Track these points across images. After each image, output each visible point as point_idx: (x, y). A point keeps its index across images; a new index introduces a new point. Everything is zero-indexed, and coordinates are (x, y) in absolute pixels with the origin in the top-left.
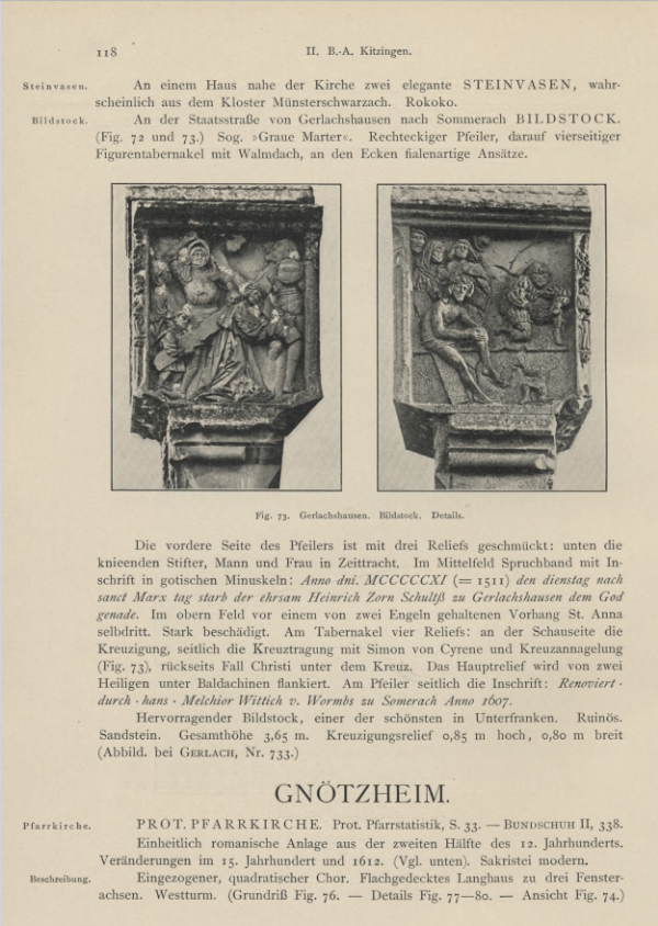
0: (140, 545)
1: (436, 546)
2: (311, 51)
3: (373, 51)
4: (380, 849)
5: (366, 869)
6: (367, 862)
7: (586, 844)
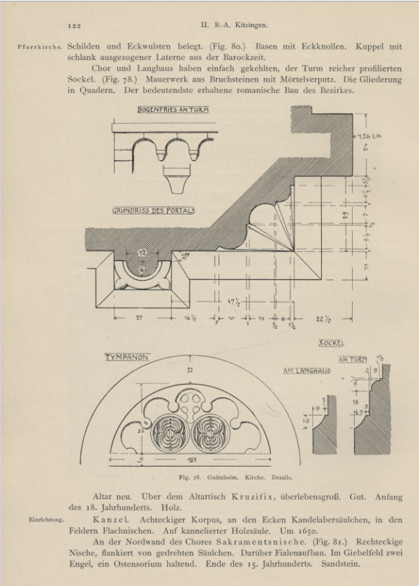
0: (347, 79)
1: (362, 542)
2: (204, 25)
3: (243, 25)
6: (338, 543)
7: (129, 508)
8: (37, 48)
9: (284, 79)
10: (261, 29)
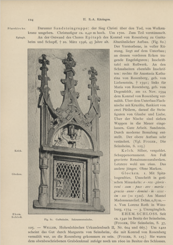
2: (84, 19)
4: (131, 138)
5: (162, 139)
8: (15, 29)
9: (58, 232)
10: (108, 21)
